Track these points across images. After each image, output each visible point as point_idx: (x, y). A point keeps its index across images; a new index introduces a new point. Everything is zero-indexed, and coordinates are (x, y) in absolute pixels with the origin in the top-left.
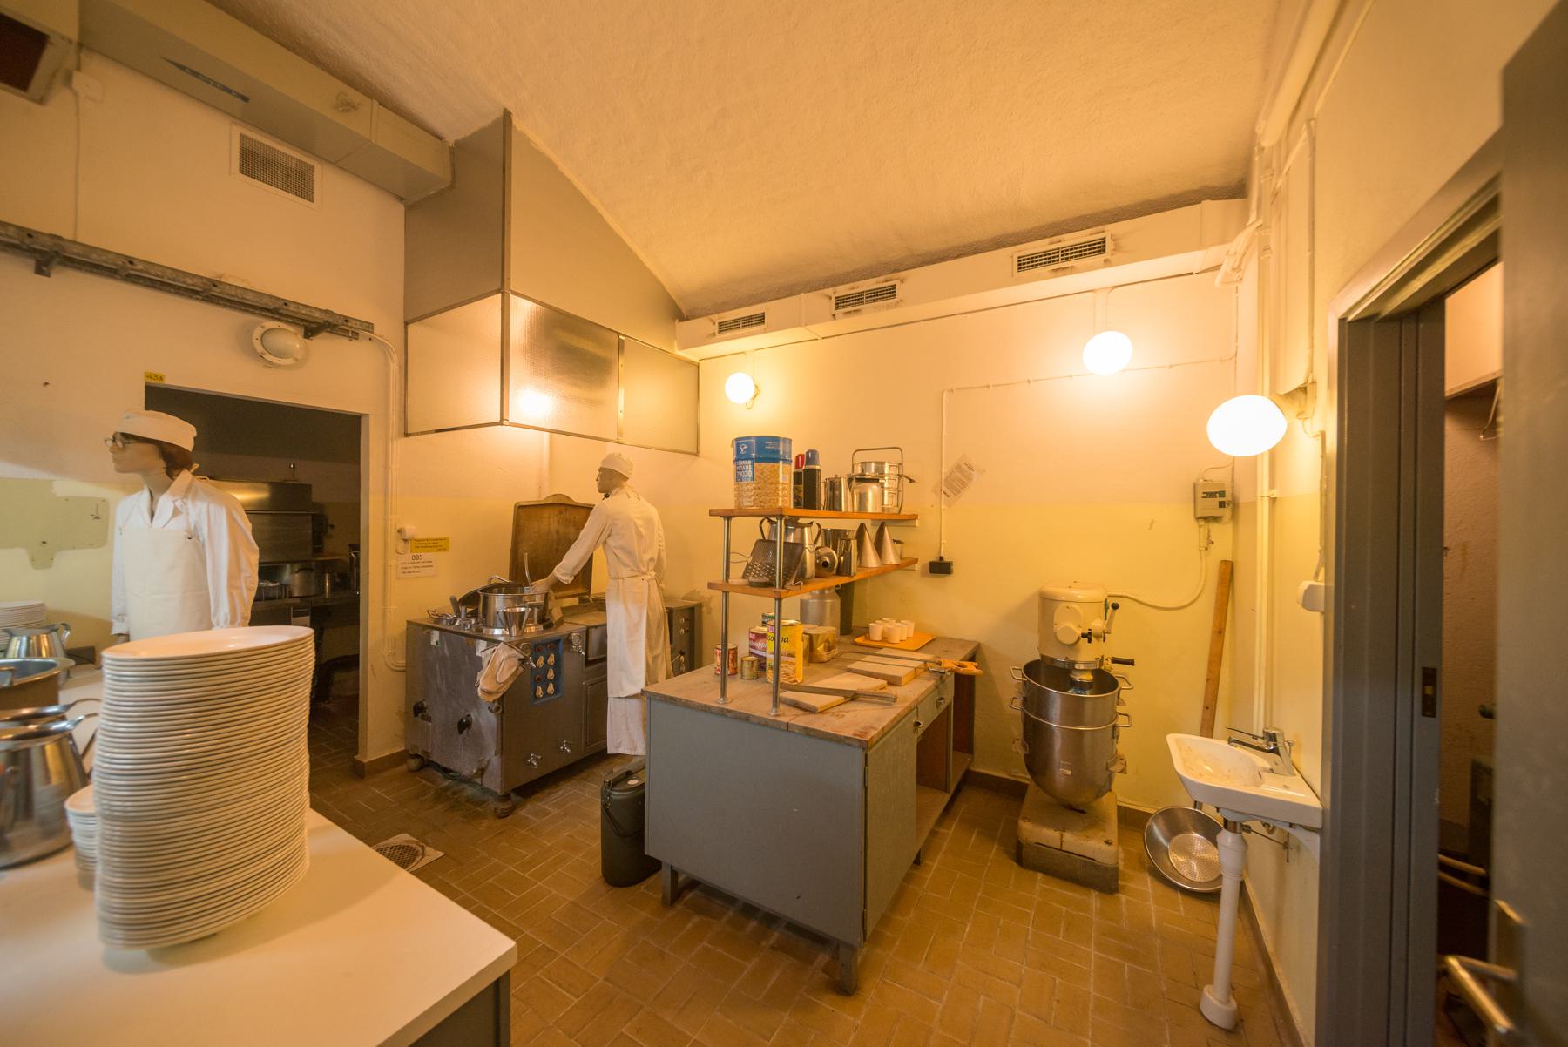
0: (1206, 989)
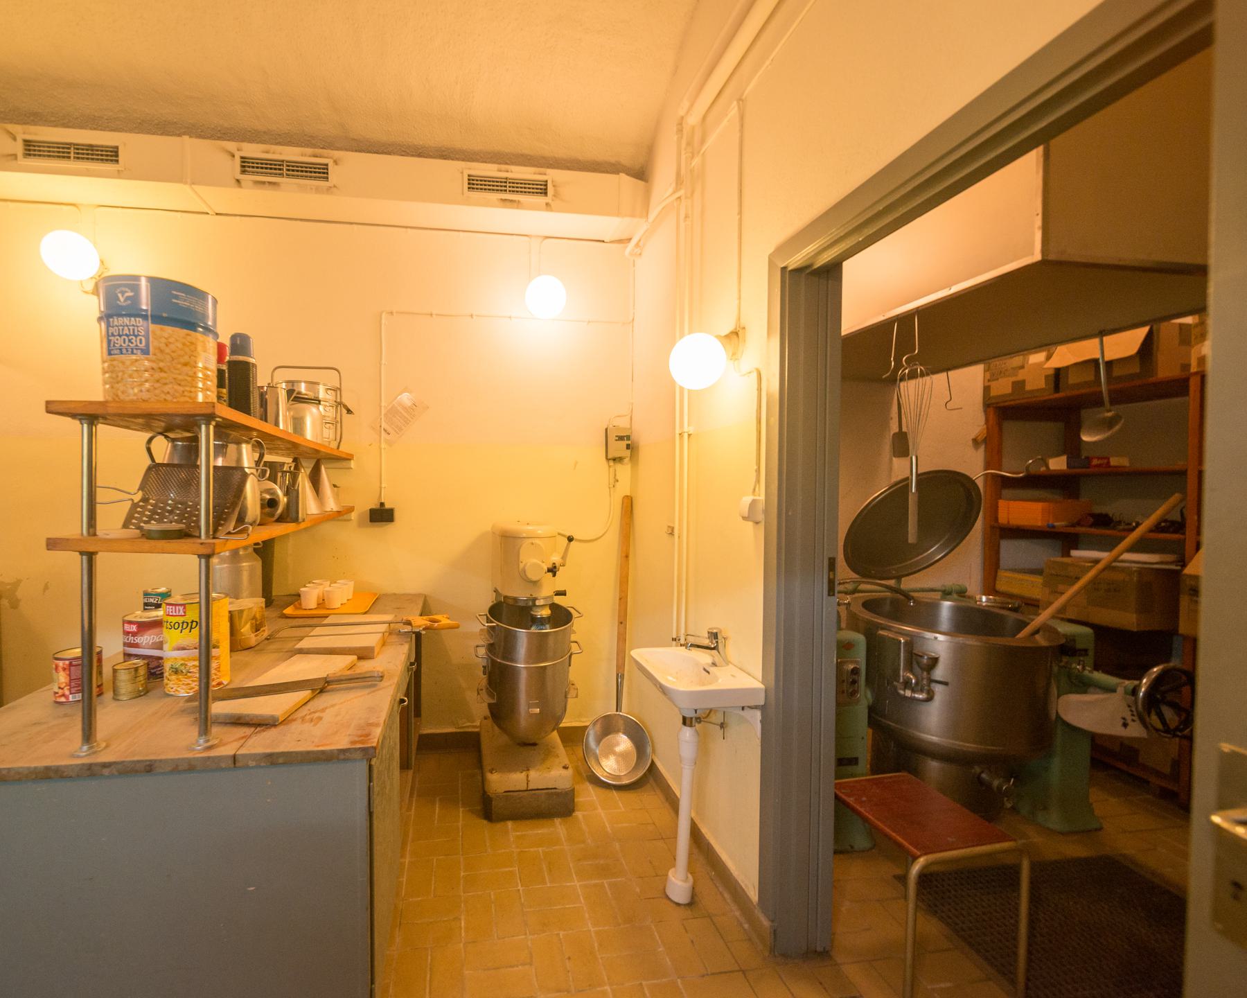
0: (671, 873)
